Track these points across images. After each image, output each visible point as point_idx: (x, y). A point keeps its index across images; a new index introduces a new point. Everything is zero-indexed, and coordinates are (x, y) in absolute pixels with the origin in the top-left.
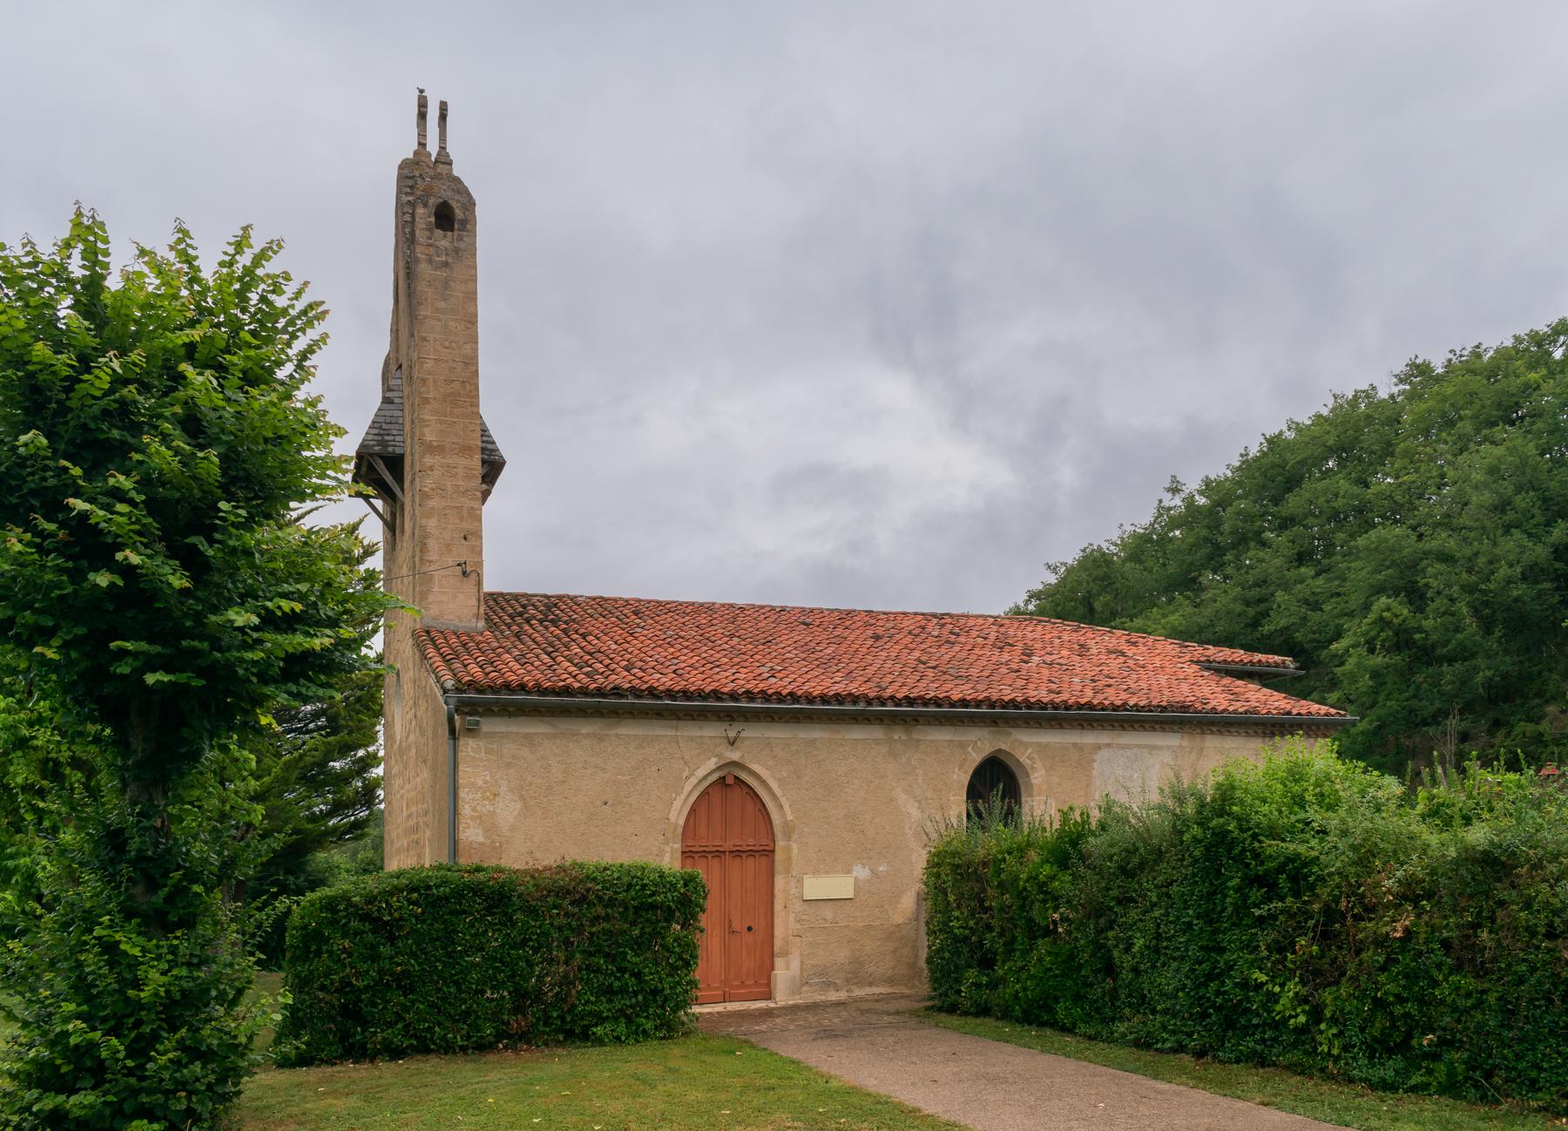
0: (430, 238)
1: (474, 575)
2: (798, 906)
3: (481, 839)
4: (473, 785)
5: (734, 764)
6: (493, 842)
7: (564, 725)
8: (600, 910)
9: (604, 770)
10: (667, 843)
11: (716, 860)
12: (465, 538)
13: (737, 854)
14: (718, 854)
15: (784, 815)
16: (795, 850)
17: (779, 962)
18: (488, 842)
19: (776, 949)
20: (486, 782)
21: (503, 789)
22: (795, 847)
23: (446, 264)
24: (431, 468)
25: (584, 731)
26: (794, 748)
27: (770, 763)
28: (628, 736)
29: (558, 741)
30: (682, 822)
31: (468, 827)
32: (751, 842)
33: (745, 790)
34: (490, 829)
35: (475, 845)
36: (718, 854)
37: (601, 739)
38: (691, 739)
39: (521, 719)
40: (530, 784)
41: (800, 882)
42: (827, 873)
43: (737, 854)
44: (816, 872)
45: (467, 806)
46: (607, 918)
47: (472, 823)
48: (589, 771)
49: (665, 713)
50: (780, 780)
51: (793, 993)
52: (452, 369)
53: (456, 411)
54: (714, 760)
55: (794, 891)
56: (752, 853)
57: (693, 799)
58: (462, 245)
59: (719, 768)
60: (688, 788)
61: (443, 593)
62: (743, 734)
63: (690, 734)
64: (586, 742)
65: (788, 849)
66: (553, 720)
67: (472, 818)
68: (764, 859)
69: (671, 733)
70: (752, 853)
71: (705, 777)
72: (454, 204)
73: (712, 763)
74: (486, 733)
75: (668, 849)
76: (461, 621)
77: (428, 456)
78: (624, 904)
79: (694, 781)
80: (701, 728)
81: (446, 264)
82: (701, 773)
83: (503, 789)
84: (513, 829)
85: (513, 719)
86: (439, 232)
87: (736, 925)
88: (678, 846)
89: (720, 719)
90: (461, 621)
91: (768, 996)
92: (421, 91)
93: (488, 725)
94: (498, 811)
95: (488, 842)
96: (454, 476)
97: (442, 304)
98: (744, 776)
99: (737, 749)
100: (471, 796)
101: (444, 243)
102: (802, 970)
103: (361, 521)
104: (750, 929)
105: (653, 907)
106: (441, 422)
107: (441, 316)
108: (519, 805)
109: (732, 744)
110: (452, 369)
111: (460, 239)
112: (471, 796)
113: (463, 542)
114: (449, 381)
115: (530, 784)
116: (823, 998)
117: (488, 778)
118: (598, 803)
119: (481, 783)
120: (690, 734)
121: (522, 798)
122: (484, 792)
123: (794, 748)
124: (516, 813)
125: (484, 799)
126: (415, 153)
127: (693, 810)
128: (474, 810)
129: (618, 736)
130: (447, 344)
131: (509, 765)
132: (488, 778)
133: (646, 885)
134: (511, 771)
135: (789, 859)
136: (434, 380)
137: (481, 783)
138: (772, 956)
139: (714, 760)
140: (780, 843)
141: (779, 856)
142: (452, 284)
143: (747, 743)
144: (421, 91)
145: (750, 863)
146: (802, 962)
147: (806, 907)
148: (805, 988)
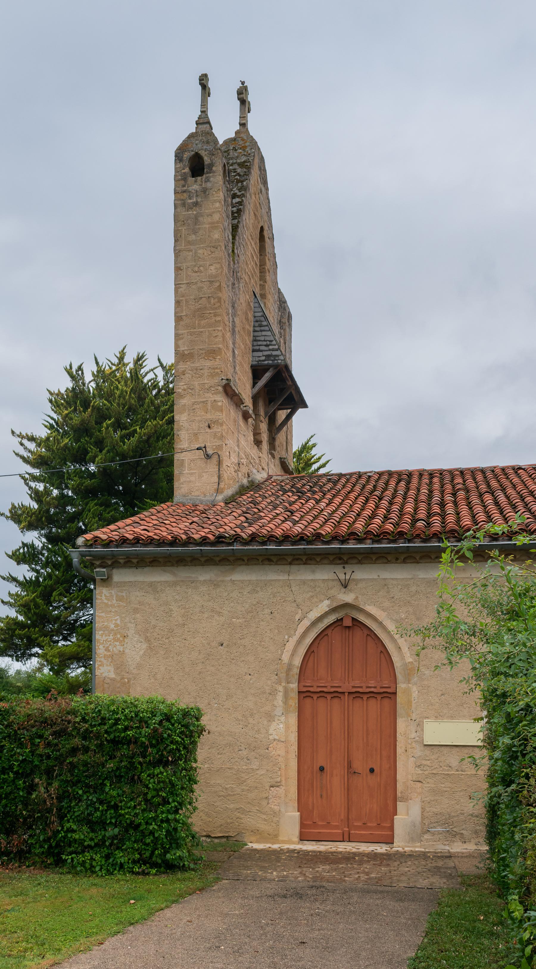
0: (184, 186)
1: (215, 458)
2: (418, 751)
3: (112, 675)
4: (106, 628)
5: (346, 606)
6: (123, 678)
7: (184, 573)
8: (77, 741)
9: (219, 614)
10: (280, 683)
11: (336, 701)
12: (209, 427)
13: (356, 695)
14: (337, 694)
15: (403, 658)
16: (415, 694)
17: (400, 806)
18: (118, 678)
19: (399, 794)
20: (116, 625)
21: (131, 632)
22: (415, 690)
23: (196, 204)
24: (184, 373)
25: (201, 578)
26: (413, 589)
27: (387, 604)
28: (242, 581)
29: (178, 588)
30: (298, 661)
31: (102, 665)
32: (372, 683)
33: (366, 632)
34: (119, 667)
35: (108, 681)
36: (337, 694)
37: (216, 585)
38: (304, 582)
39: (146, 569)
40: (155, 627)
41: (420, 725)
42: (452, 717)
43: (356, 695)
44: (439, 717)
45: (101, 647)
46: (86, 750)
47: (105, 662)
48: (206, 615)
49: (274, 559)
50: (396, 621)
51: (412, 840)
52: (200, 289)
53: (203, 322)
54: (327, 602)
55: (413, 735)
56: (372, 695)
57: (309, 640)
58: (209, 185)
59: (334, 610)
60: (301, 629)
61: (192, 474)
62: (354, 576)
63: (303, 577)
64: (204, 589)
65: (408, 692)
66: (174, 569)
67: (105, 656)
68: (386, 702)
69: (283, 577)
70: (372, 695)
71: (320, 619)
72: (203, 153)
73: (324, 606)
74: (117, 583)
75: (281, 688)
76: (205, 496)
77: (181, 363)
78: (98, 736)
79: (306, 623)
80: (313, 572)
81: (196, 204)
82: (314, 615)
83: (131, 632)
84: (139, 666)
85: (140, 570)
86: (191, 180)
87: (357, 765)
88: (294, 686)
89: (332, 563)
90: (205, 496)
91: (390, 841)
92: (243, 83)
93: (119, 576)
94: (127, 651)
95: (118, 678)
96: (201, 376)
97: (193, 237)
98: (362, 618)
99: (351, 591)
100: (104, 638)
101: (196, 187)
102: (423, 818)
103: (322, 456)
104: (372, 771)
105: (129, 742)
106: (191, 334)
107: (192, 247)
108: (145, 646)
109: (345, 587)
110: (200, 289)
111: (207, 180)
112: (104, 638)
113: (208, 430)
114: (198, 299)
115: (155, 627)
116: (447, 848)
117: (118, 622)
118: (214, 644)
119: (112, 626)
120: (303, 577)
121: (147, 640)
122: (115, 634)
123: (413, 589)
124: (141, 653)
125: (115, 640)
126: (237, 133)
127: (310, 652)
128: (107, 650)
129: (233, 581)
130: (196, 269)
131: (136, 611)
132: (118, 622)
133: (119, 719)
134: (138, 616)
135: (409, 703)
136: (187, 301)
137: (112, 626)
138: (395, 800)
139: (327, 602)
140: (401, 686)
141: (400, 698)
142: (201, 219)
143: (360, 585)
144: (243, 83)
145: (373, 703)
146: (423, 810)
147: (427, 752)
148: (426, 836)
